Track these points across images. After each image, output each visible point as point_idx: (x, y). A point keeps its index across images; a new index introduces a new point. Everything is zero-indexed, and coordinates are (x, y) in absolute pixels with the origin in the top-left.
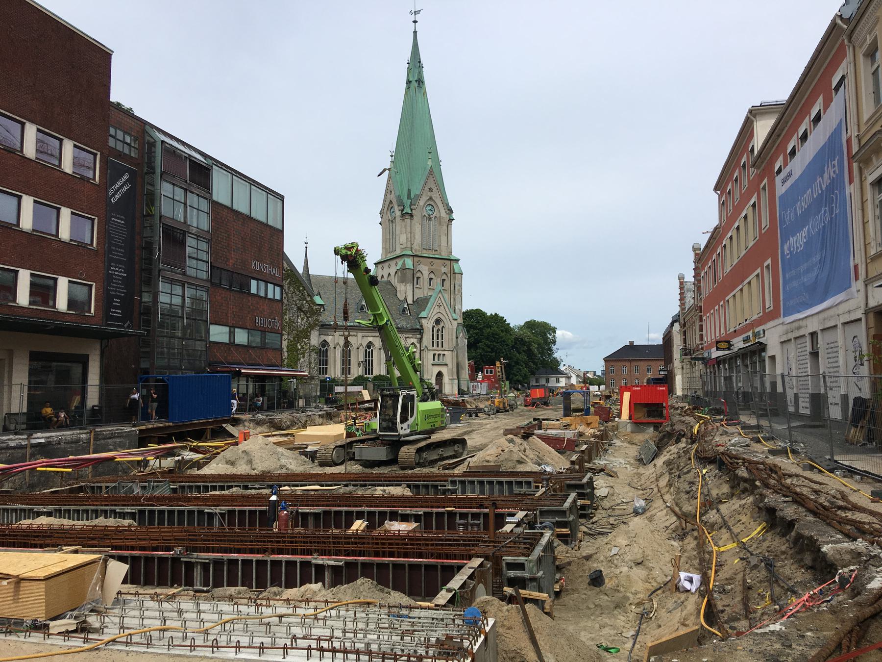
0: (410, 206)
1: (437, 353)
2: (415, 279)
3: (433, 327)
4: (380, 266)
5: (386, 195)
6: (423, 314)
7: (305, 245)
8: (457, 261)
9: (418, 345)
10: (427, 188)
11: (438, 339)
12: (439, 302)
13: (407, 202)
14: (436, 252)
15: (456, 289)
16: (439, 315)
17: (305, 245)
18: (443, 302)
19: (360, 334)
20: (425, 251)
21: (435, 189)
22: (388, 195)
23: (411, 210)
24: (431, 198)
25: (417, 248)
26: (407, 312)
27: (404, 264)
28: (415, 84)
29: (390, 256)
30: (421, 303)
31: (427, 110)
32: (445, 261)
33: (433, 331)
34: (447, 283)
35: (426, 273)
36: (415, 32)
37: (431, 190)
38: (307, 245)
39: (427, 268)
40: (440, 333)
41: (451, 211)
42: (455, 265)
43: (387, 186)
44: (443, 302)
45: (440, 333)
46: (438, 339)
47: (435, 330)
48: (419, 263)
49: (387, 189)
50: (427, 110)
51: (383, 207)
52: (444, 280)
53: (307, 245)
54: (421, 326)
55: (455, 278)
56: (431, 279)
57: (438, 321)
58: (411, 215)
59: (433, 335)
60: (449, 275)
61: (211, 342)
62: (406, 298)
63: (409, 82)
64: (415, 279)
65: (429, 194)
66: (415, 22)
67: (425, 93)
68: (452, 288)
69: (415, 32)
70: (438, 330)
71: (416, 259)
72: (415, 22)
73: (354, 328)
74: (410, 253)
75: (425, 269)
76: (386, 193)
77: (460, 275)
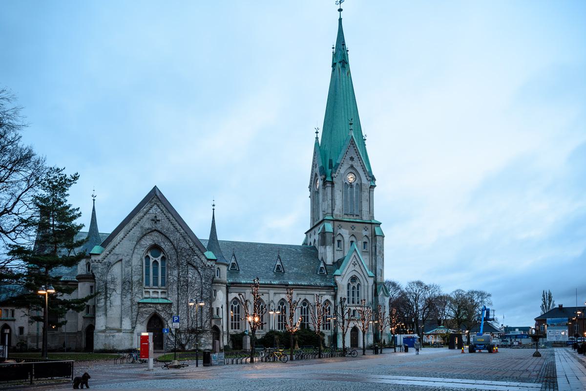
0: (331, 175)
1: (352, 309)
2: (336, 242)
3: (349, 284)
4: (309, 234)
5: (313, 169)
6: (338, 272)
7: (213, 207)
8: (379, 224)
9: (332, 302)
10: (348, 157)
11: (353, 295)
12: (354, 260)
13: (329, 171)
14: (357, 217)
15: (378, 251)
16: (354, 273)
17: (213, 207)
18: (358, 260)
19: (272, 292)
20: (346, 216)
21: (356, 158)
22: (314, 169)
23: (332, 178)
24: (352, 167)
25: (338, 213)
26: (324, 271)
27: (324, 228)
28: (339, 65)
29: (316, 223)
30: (338, 264)
31: (350, 87)
32: (367, 225)
33: (348, 288)
34: (369, 245)
35: (347, 238)
36: (340, 20)
37: (352, 159)
38: (215, 207)
39: (347, 231)
40: (356, 291)
41: (373, 179)
42: (376, 229)
43: (314, 161)
44: (358, 260)
45: (356, 291)
46: (353, 295)
47: (351, 287)
48: (340, 227)
49: (313, 164)
50: (350, 87)
51: (311, 183)
52: (365, 243)
53: (215, 207)
54: (336, 284)
55: (376, 241)
56: (352, 242)
57: (354, 279)
58: (332, 183)
59: (348, 292)
60: (370, 238)
61: (374, 342)
62: (322, 258)
63: (334, 65)
64: (336, 242)
65: (350, 163)
66: (340, 10)
67: (349, 73)
68: (374, 250)
69: (340, 20)
70: (354, 287)
71: (337, 223)
72: (340, 10)
73: (264, 286)
74: (331, 218)
75: (345, 232)
76: (313, 167)
77: (381, 238)
